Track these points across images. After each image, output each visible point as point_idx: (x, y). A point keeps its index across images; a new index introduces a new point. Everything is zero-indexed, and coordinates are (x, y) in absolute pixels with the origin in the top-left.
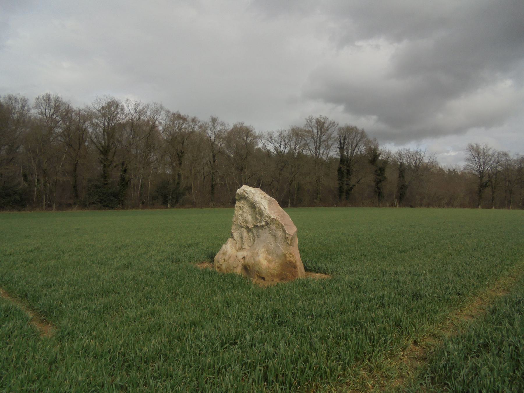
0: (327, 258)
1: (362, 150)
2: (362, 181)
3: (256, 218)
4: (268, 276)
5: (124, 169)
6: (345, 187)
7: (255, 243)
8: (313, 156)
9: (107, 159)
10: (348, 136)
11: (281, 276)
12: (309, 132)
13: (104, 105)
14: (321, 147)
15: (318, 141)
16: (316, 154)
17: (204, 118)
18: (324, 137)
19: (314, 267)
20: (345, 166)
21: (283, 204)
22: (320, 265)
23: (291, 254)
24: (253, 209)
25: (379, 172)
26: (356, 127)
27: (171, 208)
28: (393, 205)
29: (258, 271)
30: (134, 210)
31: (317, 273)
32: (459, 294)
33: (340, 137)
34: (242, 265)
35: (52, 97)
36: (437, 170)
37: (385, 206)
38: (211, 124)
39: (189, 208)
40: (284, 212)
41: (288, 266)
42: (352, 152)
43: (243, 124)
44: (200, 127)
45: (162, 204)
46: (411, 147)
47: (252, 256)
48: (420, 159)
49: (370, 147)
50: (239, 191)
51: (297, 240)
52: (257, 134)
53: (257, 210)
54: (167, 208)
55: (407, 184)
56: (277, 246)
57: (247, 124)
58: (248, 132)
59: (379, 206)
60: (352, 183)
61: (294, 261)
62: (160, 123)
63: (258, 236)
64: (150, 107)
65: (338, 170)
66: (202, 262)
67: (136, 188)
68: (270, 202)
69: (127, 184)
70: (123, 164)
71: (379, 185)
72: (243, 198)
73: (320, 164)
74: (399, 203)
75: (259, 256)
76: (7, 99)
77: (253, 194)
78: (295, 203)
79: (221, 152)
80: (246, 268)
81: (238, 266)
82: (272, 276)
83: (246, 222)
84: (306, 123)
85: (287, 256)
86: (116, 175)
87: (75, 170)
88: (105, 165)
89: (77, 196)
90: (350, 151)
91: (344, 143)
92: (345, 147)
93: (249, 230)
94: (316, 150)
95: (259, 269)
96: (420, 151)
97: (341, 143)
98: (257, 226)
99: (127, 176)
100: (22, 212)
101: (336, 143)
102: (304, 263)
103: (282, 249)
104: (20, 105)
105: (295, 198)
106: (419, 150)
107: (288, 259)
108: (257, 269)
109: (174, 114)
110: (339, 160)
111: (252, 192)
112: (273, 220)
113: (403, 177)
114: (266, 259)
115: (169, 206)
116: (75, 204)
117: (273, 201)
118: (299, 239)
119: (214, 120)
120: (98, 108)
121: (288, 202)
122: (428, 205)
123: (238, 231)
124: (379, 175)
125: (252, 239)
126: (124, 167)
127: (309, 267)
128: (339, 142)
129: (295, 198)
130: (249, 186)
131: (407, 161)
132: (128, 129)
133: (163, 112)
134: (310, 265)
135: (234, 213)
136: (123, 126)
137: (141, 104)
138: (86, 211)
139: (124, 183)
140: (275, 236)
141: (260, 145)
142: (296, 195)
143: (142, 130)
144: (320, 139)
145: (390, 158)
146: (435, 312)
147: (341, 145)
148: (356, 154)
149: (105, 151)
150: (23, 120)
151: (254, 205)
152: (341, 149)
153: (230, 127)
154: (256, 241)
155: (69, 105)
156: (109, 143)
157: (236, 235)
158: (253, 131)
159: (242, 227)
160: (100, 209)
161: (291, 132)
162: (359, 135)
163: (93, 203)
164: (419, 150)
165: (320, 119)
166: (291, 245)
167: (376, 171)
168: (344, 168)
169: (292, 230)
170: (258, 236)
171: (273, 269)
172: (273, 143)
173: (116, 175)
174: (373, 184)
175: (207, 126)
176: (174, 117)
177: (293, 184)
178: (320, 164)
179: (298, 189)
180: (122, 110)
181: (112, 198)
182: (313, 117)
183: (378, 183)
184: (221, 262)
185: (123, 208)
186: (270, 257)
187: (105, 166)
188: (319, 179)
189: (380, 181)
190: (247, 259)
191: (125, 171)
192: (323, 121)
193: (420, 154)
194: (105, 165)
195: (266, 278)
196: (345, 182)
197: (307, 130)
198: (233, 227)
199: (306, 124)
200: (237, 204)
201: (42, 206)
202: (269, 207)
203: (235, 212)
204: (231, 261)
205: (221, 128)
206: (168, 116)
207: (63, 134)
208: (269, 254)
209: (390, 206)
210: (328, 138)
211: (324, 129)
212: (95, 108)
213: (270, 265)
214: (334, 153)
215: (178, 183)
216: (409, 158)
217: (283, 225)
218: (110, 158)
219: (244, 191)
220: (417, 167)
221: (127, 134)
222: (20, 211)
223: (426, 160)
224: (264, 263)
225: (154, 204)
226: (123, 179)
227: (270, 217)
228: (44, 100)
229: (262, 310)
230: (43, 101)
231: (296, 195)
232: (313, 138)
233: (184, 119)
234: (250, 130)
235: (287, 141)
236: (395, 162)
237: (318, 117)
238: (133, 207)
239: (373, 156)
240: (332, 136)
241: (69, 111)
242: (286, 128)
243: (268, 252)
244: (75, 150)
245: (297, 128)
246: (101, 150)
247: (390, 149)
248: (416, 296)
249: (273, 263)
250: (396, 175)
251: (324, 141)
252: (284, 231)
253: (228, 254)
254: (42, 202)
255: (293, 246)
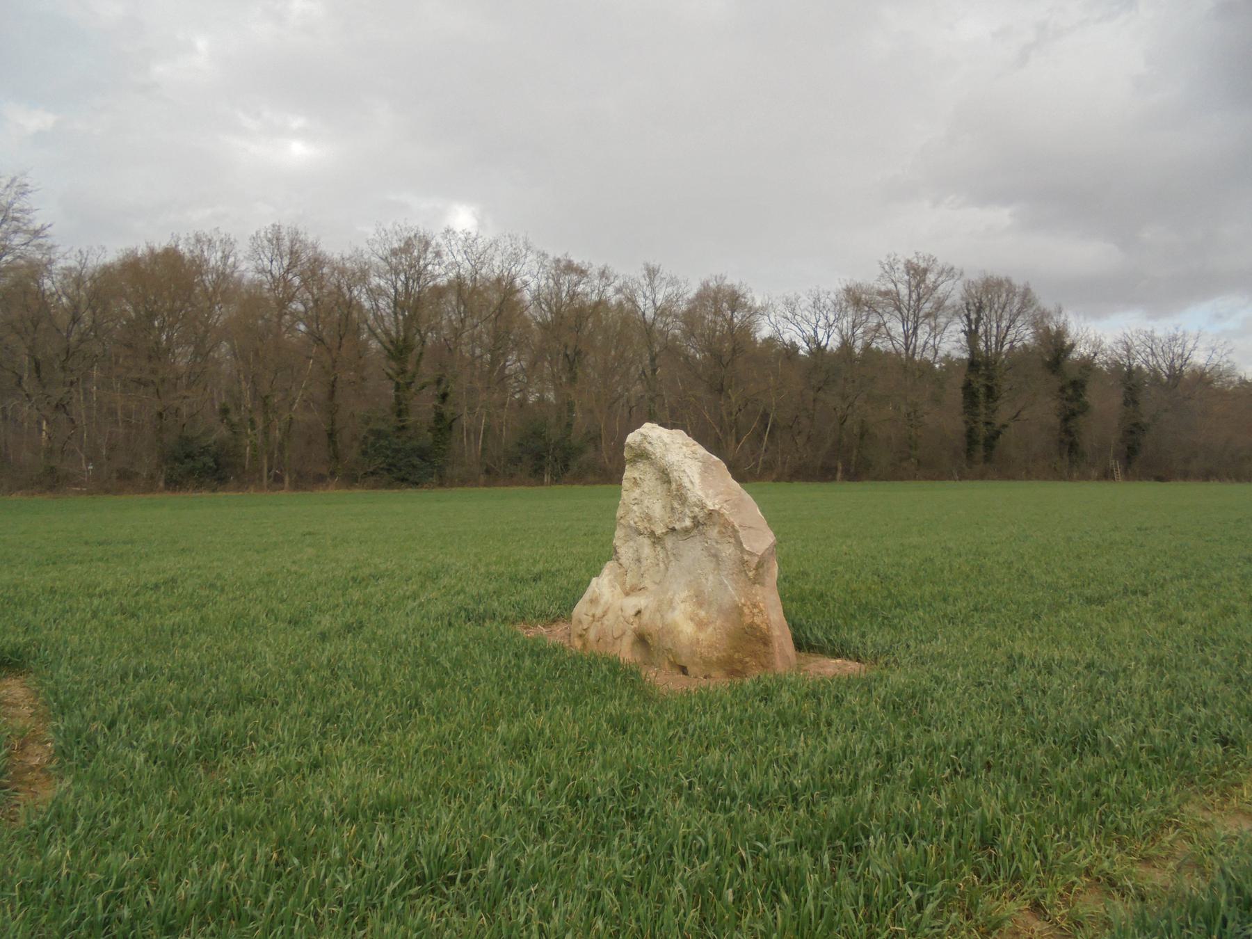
0: (873, 616)
1: (1024, 335)
2: (1025, 414)
3: (672, 509)
4: (696, 664)
5: (441, 392)
6: (982, 431)
7: (669, 573)
8: (899, 354)
9: (404, 372)
10: (987, 299)
11: (733, 668)
12: (886, 294)
13: (396, 245)
14: (919, 332)
15: (911, 317)
16: (907, 349)
17: (627, 271)
18: (927, 307)
19: (830, 641)
20: (981, 376)
21: (740, 475)
22: (844, 634)
23: (755, 606)
24: (665, 486)
25: (1070, 392)
26: (1008, 281)
27: (552, 483)
28: (1107, 475)
29: (669, 650)
30: (466, 489)
31: (838, 656)
32: (1224, 742)
33: (968, 304)
34: (635, 631)
35: (284, 232)
36: (1231, 382)
37: (1085, 477)
38: (644, 282)
39: (595, 483)
40: (743, 492)
41: (750, 639)
42: (1000, 342)
43: (723, 278)
44: (618, 291)
45: (530, 475)
46: (1162, 328)
47: (658, 609)
48: (1182, 355)
49: (1047, 330)
50: (632, 438)
51: (776, 570)
52: (758, 304)
53: (674, 486)
54: (542, 484)
55: (1145, 420)
56: (721, 583)
57: (732, 280)
58: (735, 299)
59: (1070, 478)
60: (1000, 419)
61: (764, 626)
62: (526, 284)
63: (678, 557)
64: (501, 246)
65: (964, 388)
66: (554, 621)
67: (472, 437)
68: (706, 468)
69: (450, 428)
70: (439, 382)
71: (1071, 424)
72: (642, 455)
73: (918, 373)
74: (1125, 471)
75: (674, 609)
76: (193, 241)
77: (665, 445)
78: (852, 470)
79: (671, 349)
80: (642, 640)
81: (624, 633)
82: (707, 663)
83: (649, 518)
84: (880, 271)
85: (746, 611)
86: (423, 407)
87: (332, 394)
88: (398, 384)
89: (336, 457)
90: (993, 339)
91: (978, 320)
92: (981, 330)
93: (656, 540)
94: (907, 337)
95: (674, 644)
96: (1184, 335)
97: (969, 320)
98: (673, 530)
99: (448, 410)
100: (220, 494)
101: (957, 320)
102: (795, 626)
103: (732, 592)
104: (220, 254)
105: (854, 458)
106: (1180, 334)
107: (748, 620)
108: (670, 645)
109: (558, 261)
110: (967, 363)
111: (662, 441)
112: (711, 513)
113: (1135, 402)
114: (692, 620)
115: (547, 478)
116: (333, 474)
117: (714, 463)
118: (781, 563)
119: (652, 273)
120: (380, 252)
121: (836, 468)
122: (1207, 476)
123: (631, 543)
124: (1069, 399)
125: (662, 565)
126: (443, 386)
127: (817, 639)
128: (964, 319)
129: (854, 458)
130: (661, 425)
131: (1147, 362)
132: (453, 298)
133: (531, 257)
134: (820, 635)
135: (620, 495)
136: (439, 292)
137: (480, 240)
138: (358, 492)
139: (443, 425)
140: (716, 557)
141: (764, 331)
142: (855, 451)
143: (490, 302)
144: (918, 308)
145: (1100, 356)
146: (1131, 802)
147: (970, 326)
148: (1012, 347)
149: (399, 350)
150: (226, 286)
151: (667, 475)
152: (971, 335)
153: (692, 290)
154: (671, 569)
155: (315, 248)
156: (407, 330)
157: (625, 552)
158: (749, 296)
159: (641, 534)
160: (389, 486)
161: (841, 296)
162: (1016, 300)
163: (373, 473)
164: (1180, 334)
165: (915, 261)
166: (757, 580)
167: (1062, 390)
168: (979, 383)
169: (761, 540)
170: (678, 557)
171: (710, 647)
172: (797, 325)
173: (423, 407)
174: (1055, 421)
175: (636, 286)
176: (557, 268)
177: (848, 422)
178: (918, 373)
179: (862, 436)
180: (438, 254)
181: (416, 461)
182: (899, 257)
183: (1066, 420)
184: (586, 620)
185: (441, 485)
186: (702, 613)
187: (398, 387)
188: (915, 412)
189: (1074, 414)
190: (646, 617)
191: (444, 397)
192: (923, 265)
193: (1184, 346)
194: (398, 384)
195: (692, 670)
196: (982, 418)
197: (883, 289)
198: (619, 533)
199: (882, 276)
200: (629, 473)
201: (261, 479)
202: (703, 480)
203: (624, 493)
204: (609, 621)
205: (670, 290)
206: (542, 265)
207: (307, 318)
208: (700, 604)
209: (1098, 479)
210: (938, 309)
211: (927, 287)
212: (374, 253)
213: (702, 636)
214: (950, 343)
215: (569, 425)
216: (1153, 354)
217: (737, 526)
218: (409, 367)
219: (645, 437)
220: (1176, 375)
221: (450, 310)
222: (214, 491)
223: (1199, 359)
224: (687, 629)
225: (512, 476)
226: (440, 417)
227: (703, 507)
228: (270, 241)
229: (595, 775)
230: (266, 243)
231: (855, 451)
232: (899, 309)
233: (582, 273)
234: (741, 293)
235: (832, 317)
236: (1116, 367)
237: (911, 256)
238: (464, 482)
239: (1054, 350)
240: (948, 303)
241: (318, 262)
242: (833, 285)
243: (700, 599)
244: (329, 350)
245: (859, 286)
246: (389, 351)
247: (1099, 333)
248: (1083, 742)
249: (710, 629)
250: (1117, 400)
251: (927, 315)
252: (739, 544)
253: (602, 602)
254: (261, 470)
255: (763, 585)
